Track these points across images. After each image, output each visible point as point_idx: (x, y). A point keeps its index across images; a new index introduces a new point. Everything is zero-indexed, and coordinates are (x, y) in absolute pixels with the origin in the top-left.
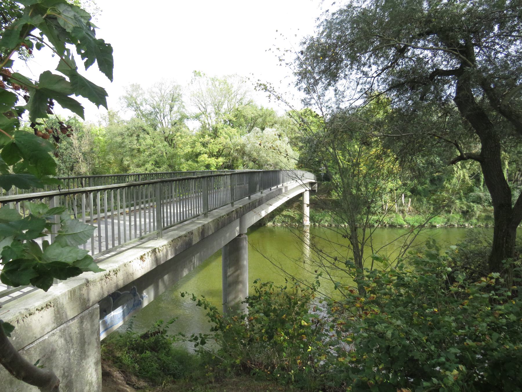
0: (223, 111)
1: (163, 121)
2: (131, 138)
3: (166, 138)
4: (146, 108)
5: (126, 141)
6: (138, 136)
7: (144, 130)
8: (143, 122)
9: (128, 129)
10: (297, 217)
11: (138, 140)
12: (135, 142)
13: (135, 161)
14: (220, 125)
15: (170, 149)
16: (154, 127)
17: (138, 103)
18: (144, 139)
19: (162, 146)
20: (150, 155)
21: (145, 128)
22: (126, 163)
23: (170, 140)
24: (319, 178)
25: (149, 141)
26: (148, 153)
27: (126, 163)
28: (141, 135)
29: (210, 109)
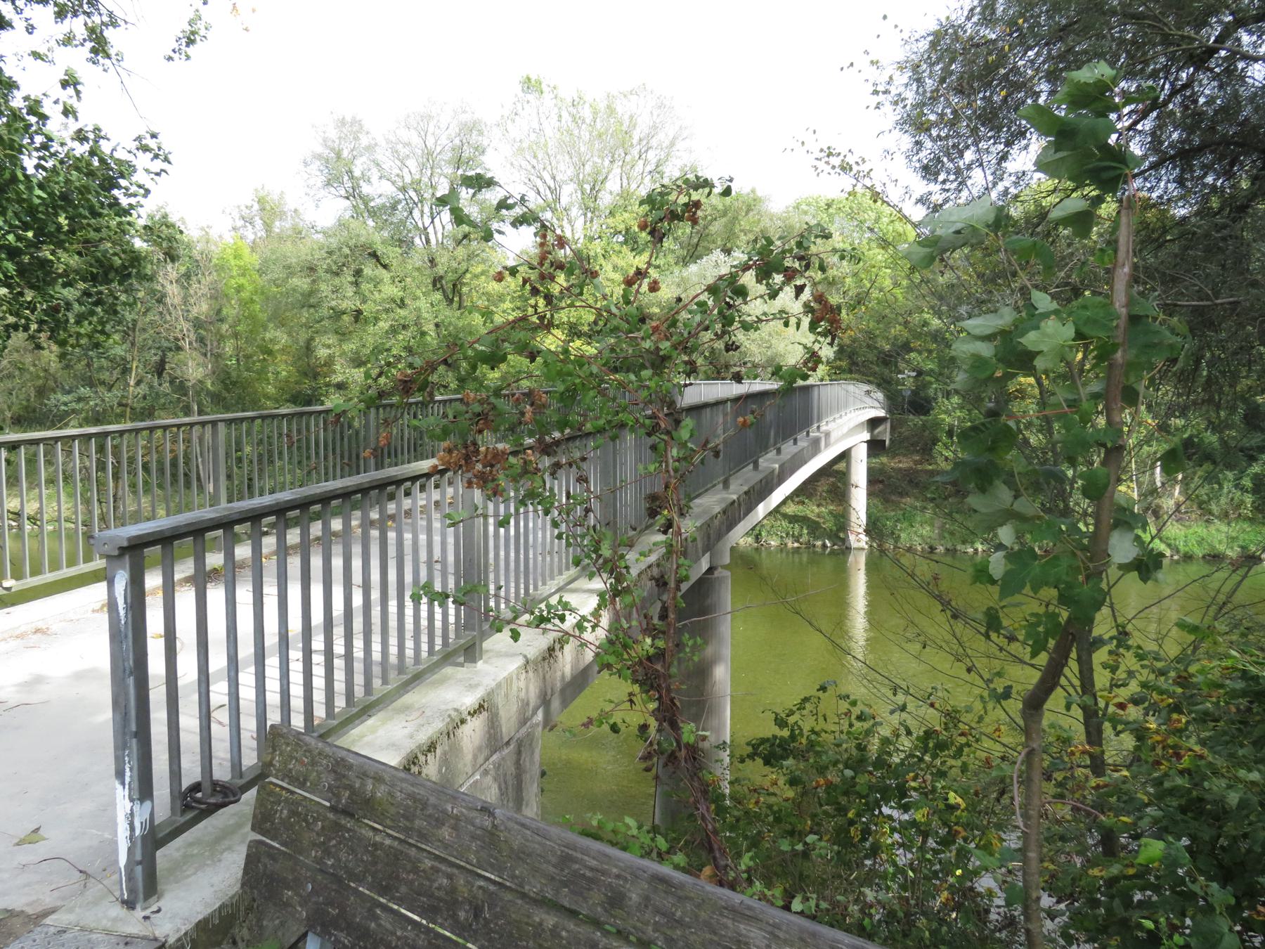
0: (606, 200)
1: (430, 230)
2: (337, 281)
3: (437, 282)
4: (379, 190)
5: (323, 287)
6: (358, 273)
7: (374, 255)
8: (369, 231)
9: (330, 253)
10: (829, 525)
11: (356, 284)
12: (350, 291)
13: (350, 346)
14: (597, 248)
15: (448, 314)
16: (404, 243)
17: (357, 173)
18: (377, 283)
19: (426, 305)
20: (393, 331)
21: (380, 250)
22: (322, 353)
23: (450, 288)
24: (894, 401)
25: (390, 290)
26: (384, 325)
27: (322, 353)
28: (368, 271)
29: (569, 194)
